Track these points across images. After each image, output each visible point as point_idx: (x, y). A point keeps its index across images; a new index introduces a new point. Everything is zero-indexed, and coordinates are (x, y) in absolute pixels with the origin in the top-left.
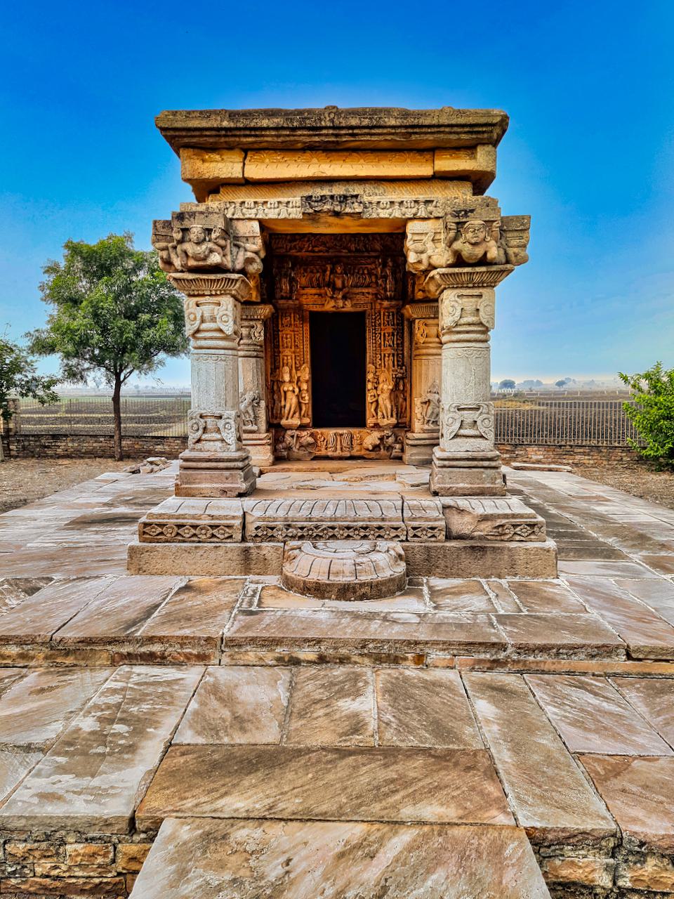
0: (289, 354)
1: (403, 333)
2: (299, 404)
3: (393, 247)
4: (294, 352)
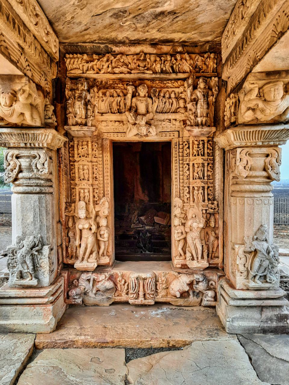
0: (86, 187)
1: (214, 164)
2: (98, 242)
3: (205, 67)
4: (92, 185)
